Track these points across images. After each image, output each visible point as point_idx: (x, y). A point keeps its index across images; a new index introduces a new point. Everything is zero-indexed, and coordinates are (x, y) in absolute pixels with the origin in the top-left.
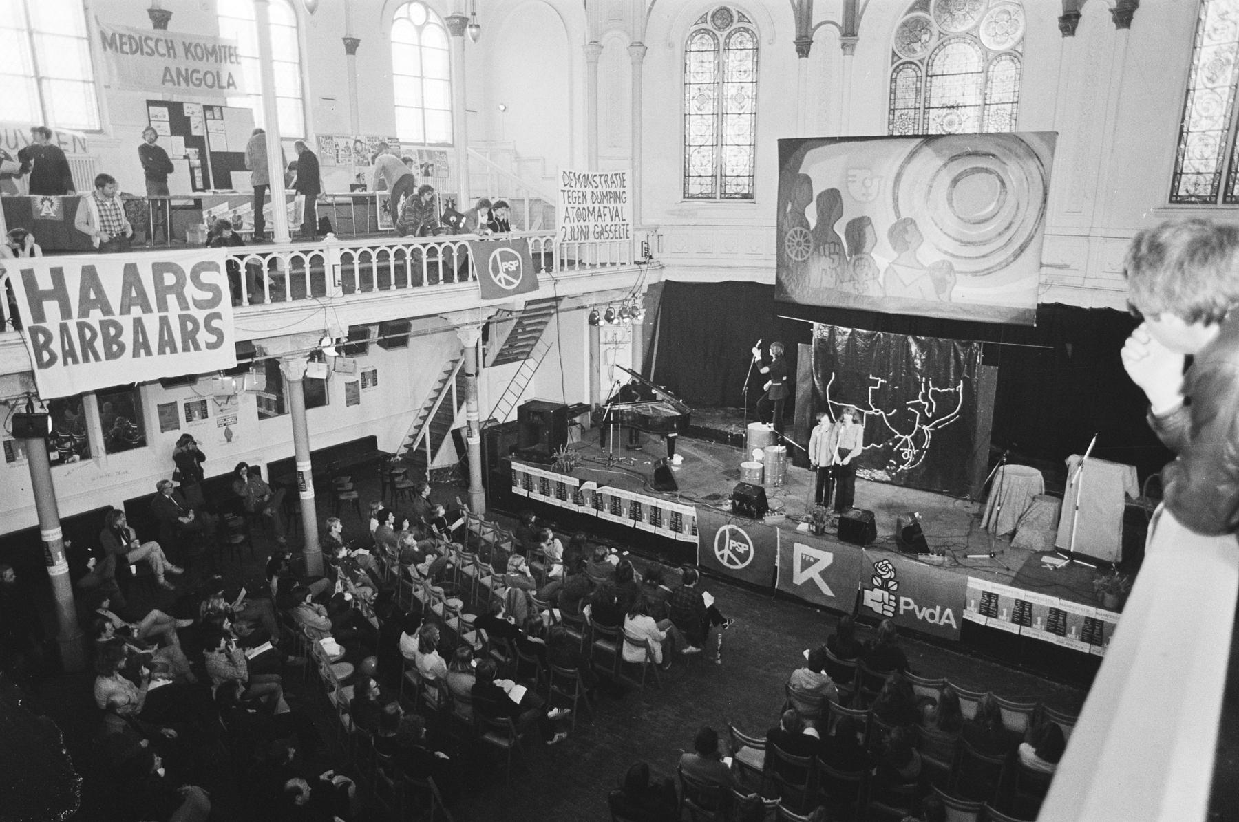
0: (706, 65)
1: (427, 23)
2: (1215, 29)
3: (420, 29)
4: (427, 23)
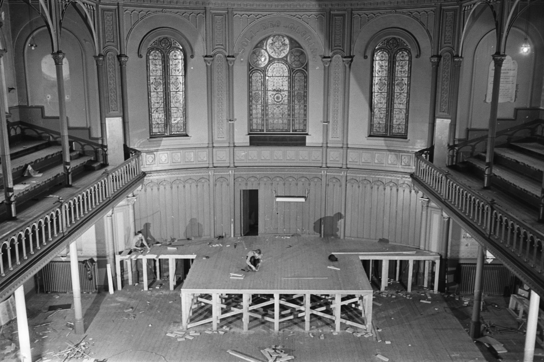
0: (158, 66)
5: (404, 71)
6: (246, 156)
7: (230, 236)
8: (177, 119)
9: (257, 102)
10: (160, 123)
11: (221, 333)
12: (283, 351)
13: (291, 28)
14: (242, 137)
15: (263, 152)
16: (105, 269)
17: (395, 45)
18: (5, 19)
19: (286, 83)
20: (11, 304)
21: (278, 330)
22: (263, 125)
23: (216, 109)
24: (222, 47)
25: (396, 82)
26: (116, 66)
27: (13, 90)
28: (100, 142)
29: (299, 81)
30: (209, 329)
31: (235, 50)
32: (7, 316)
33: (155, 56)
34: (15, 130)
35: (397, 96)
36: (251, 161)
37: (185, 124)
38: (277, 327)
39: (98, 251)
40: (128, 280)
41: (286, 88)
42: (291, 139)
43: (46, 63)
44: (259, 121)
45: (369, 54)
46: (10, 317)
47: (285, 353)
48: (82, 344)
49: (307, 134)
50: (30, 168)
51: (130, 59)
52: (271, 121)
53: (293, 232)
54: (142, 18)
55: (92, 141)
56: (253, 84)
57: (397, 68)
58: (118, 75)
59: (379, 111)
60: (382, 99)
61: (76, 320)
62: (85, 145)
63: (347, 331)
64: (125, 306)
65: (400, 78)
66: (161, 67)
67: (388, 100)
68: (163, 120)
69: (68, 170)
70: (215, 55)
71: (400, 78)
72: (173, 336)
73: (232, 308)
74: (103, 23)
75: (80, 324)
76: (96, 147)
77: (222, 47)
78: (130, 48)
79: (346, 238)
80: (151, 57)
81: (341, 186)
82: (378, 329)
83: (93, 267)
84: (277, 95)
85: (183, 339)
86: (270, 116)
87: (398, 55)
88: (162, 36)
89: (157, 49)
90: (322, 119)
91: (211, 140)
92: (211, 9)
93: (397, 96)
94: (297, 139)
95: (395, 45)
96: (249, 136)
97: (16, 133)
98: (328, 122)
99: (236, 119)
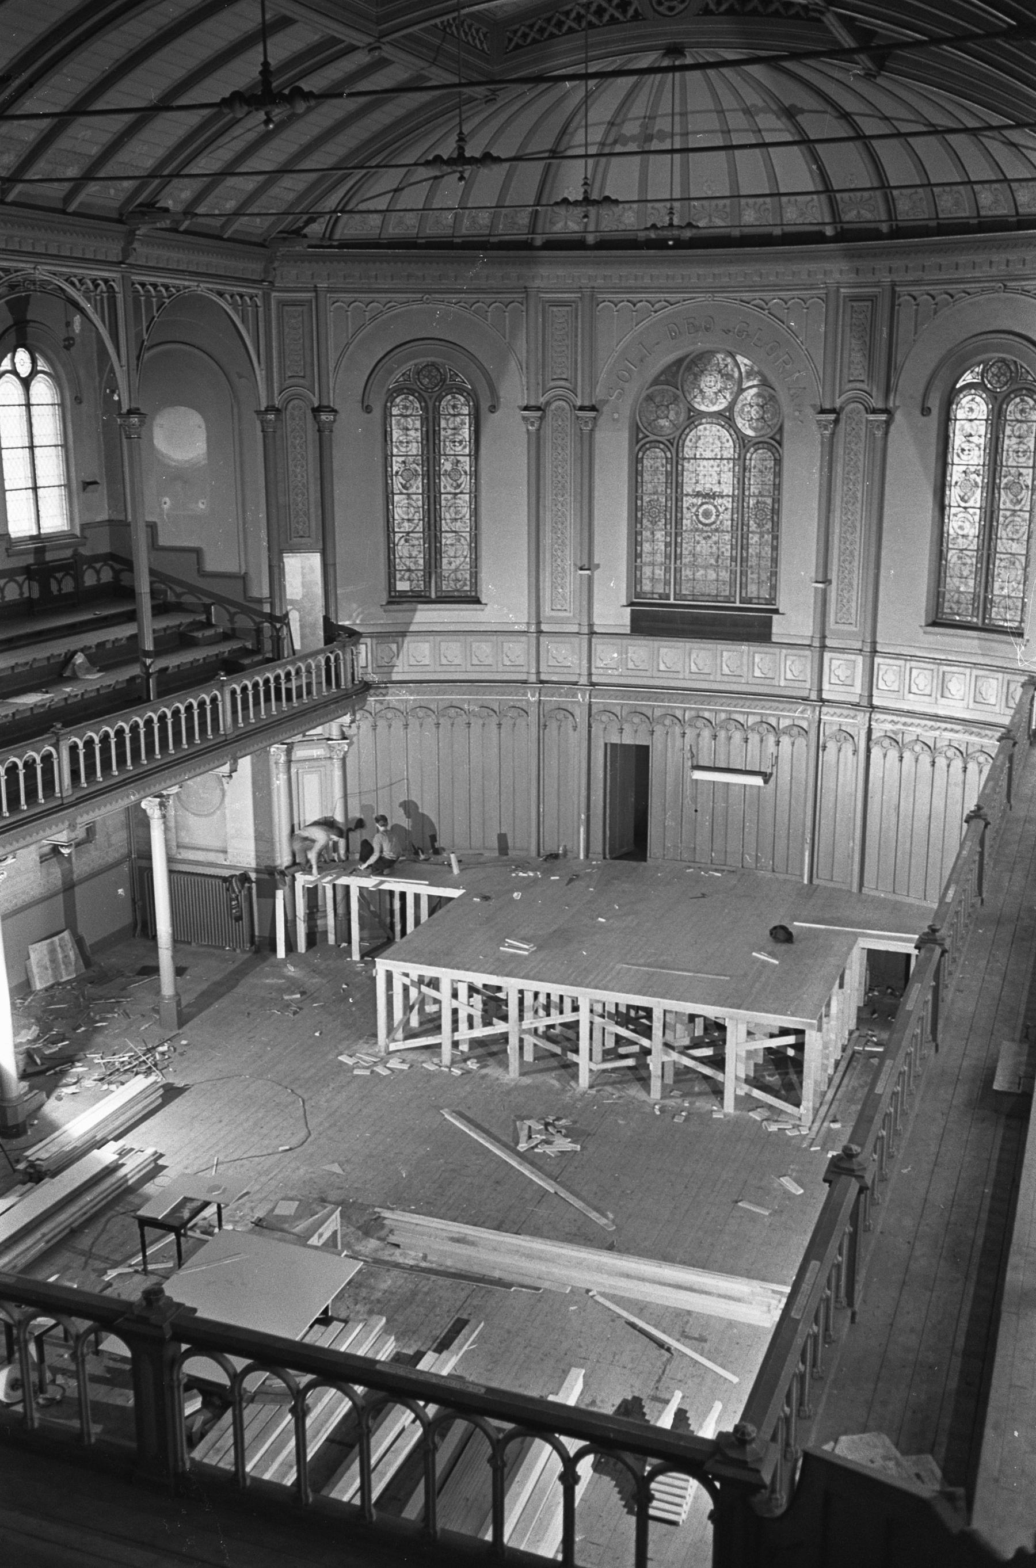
0: (412, 433)
1: (34, 372)
2: (963, 450)
3: (26, 383)
4: (34, 372)
5: (1025, 452)
6: (623, 662)
7: (578, 857)
8: (455, 558)
9: (654, 523)
10: (413, 568)
11: (456, 1072)
12: (564, 1131)
13: (740, 333)
14: (613, 612)
15: (663, 651)
16: (271, 900)
17: (1003, 379)
18: (82, 330)
19: (728, 477)
20: (59, 949)
21: (587, 1085)
22: (667, 583)
23: (547, 539)
24: (567, 385)
25: (1004, 481)
26: (310, 432)
27: (91, 487)
28: (267, 609)
29: (761, 471)
30: (436, 1060)
31: (600, 392)
32: (50, 972)
33: (406, 408)
34: (98, 572)
35: (1006, 518)
36: (477, 668)
37: (475, 575)
38: (584, 1079)
39: (257, 857)
40: (326, 932)
41: (728, 490)
42: (735, 622)
43: (162, 426)
44: (657, 572)
45: (935, 403)
46: (55, 976)
47: (566, 1136)
48: (161, 1049)
49: (776, 611)
50: (79, 659)
51: (342, 416)
52: (687, 573)
53: (733, 862)
54: (373, 318)
55: (249, 607)
56: (646, 477)
57: (1007, 442)
58: (312, 452)
59: (960, 558)
60: (967, 525)
61: (163, 998)
62: (236, 613)
63: (751, 1114)
64: (293, 985)
65: (1013, 471)
66: (419, 434)
67: (982, 528)
68: (421, 562)
69: (148, 668)
70: (548, 403)
71: (1013, 471)
72: (350, 1061)
73: (495, 1020)
74: (281, 333)
75: (170, 1012)
76: (258, 619)
77: (567, 385)
78: (344, 389)
79: (865, 890)
80: (395, 411)
81: (855, 752)
82: (834, 1121)
83: (244, 892)
84: (705, 507)
85: (367, 1073)
86: (685, 561)
87: (1011, 408)
88: (423, 361)
89: (411, 392)
90: (813, 574)
91: (534, 614)
92: (539, 290)
93: (1006, 518)
94: (749, 623)
95: (1003, 379)
96: (629, 609)
97: (99, 579)
98: (826, 581)
99: (598, 566)
